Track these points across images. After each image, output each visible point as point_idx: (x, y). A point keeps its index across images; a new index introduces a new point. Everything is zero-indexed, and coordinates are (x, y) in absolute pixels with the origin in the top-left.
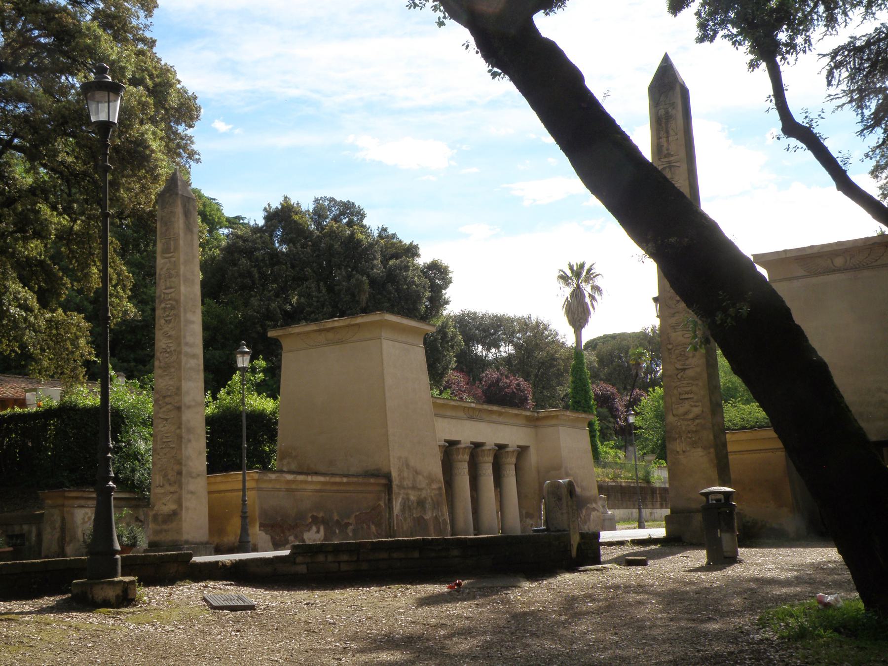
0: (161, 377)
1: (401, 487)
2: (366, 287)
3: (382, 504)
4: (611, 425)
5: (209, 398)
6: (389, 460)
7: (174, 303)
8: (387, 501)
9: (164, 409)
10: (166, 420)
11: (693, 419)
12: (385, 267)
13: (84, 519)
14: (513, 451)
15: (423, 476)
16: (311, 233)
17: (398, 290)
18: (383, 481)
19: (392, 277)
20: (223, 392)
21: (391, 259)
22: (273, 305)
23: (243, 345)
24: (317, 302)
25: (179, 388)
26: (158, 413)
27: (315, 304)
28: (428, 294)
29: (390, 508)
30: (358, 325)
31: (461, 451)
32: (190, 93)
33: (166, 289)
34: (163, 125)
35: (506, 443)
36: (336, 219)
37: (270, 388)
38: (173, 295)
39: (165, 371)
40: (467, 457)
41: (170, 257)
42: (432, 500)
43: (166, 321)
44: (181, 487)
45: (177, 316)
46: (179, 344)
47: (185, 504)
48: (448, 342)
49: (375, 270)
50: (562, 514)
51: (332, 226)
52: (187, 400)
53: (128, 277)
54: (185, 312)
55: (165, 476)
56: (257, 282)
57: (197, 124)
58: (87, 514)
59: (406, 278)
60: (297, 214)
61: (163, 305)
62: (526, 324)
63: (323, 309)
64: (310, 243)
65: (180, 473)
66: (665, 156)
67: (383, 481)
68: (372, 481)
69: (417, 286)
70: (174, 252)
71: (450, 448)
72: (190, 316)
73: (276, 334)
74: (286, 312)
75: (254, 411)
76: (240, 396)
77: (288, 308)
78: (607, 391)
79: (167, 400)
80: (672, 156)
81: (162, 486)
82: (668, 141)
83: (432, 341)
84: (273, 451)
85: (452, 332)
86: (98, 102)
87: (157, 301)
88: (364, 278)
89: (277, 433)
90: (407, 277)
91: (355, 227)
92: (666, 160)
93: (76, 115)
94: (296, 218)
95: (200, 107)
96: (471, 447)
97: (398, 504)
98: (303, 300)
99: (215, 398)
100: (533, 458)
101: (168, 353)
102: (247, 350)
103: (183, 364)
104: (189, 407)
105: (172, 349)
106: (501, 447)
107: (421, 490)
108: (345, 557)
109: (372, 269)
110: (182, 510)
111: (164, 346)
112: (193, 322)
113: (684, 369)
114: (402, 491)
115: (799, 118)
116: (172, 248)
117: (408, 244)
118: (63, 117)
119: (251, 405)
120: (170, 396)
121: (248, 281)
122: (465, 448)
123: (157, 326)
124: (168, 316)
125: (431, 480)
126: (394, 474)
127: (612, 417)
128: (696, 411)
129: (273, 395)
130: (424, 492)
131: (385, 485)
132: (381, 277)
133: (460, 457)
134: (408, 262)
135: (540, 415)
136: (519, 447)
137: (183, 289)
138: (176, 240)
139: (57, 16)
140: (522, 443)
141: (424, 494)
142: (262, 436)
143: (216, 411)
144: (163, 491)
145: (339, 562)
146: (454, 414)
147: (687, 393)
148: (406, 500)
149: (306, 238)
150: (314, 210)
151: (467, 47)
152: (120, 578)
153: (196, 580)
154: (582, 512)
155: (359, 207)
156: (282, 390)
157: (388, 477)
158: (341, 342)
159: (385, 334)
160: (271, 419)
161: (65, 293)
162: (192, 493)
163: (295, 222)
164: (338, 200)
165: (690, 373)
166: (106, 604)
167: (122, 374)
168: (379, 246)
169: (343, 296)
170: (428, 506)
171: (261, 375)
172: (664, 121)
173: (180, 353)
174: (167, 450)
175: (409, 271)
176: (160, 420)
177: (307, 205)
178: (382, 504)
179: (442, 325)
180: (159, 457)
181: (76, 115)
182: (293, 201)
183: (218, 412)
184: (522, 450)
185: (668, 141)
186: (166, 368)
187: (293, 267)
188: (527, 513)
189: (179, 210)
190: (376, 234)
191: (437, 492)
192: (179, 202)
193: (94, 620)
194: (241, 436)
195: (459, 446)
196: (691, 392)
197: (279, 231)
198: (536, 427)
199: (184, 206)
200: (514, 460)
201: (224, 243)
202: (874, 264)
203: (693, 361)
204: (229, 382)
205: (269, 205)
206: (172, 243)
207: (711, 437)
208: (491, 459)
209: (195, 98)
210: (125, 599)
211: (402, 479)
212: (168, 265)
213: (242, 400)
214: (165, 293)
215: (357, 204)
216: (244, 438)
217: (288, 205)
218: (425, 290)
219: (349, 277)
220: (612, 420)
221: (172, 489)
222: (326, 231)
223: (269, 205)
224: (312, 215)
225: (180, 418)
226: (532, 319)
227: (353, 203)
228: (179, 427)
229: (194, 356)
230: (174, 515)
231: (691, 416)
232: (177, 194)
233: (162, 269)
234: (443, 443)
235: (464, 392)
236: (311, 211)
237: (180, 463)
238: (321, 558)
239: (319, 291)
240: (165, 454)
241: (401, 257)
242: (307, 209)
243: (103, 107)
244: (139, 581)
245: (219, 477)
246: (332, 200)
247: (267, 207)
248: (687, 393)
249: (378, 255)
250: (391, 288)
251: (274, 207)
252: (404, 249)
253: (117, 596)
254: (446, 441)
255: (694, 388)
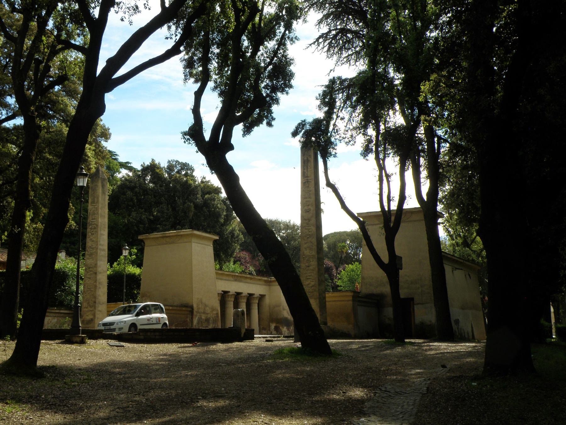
0: (88, 259)
1: (198, 312)
2: (193, 209)
3: (188, 320)
4: (329, 284)
5: (108, 266)
6: (193, 299)
7: (95, 226)
8: (191, 319)
9: (89, 273)
10: (90, 278)
11: (311, 287)
12: (203, 199)
13: (48, 322)
14: (257, 297)
15: (209, 308)
16: (165, 179)
17: (209, 211)
18: (189, 309)
19: (206, 204)
20: (115, 263)
21: (206, 194)
22: (144, 216)
23: (126, 245)
24: (167, 215)
25: (96, 264)
26: (86, 275)
27: (166, 217)
28: (225, 213)
29: (192, 322)
30: (181, 235)
31: (230, 296)
32: (107, 127)
33: (92, 219)
34: (94, 145)
35: (253, 293)
36: (179, 172)
37: (139, 263)
38: (95, 222)
39: (90, 256)
40: (233, 299)
41: (95, 205)
42: (213, 319)
43: (92, 234)
44: (95, 308)
45: (97, 232)
46: (97, 245)
47: (97, 316)
48: (235, 238)
49: (198, 200)
50: (239, 321)
51: (176, 176)
52: (99, 269)
53: (72, 209)
54: (101, 230)
55: (88, 303)
56: (136, 204)
57: (109, 141)
58: (49, 320)
59: (213, 205)
60: (158, 169)
61: (90, 227)
62: (288, 226)
63: (170, 219)
64: (164, 185)
65: (95, 302)
66: (306, 177)
67: (189, 309)
68: (184, 309)
69: (219, 209)
70: (97, 203)
71: (224, 295)
72: (102, 232)
73: (142, 238)
74: (150, 219)
75: (130, 274)
76: (124, 266)
77: (152, 217)
78: (329, 265)
79: (91, 269)
80: (309, 177)
81: (87, 308)
82: (307, 171)
83: (226, 238)
84: (138, 293)
85: (238, 233)
86: (80, 178)
87: (88, 225)
88: (192, 204)
89: (140, 284)
90: (214, 204)
91: (188, 177)
92: (306, 178)
93: (55, 141)
94: (158, 171)
95: (111, 134)
96: (235, 295)
97: (196, 320)
98: (159, 214)
99: (111, 267)
100: (267, 301)
101: (92, 248)
102: (127, 248)
103: (98, 253)
104: (100, 273)
105: (94, 247)
106: (251, 295)
107: (208, 314)
108: (157, 334)
109: (196, 200)
110: (95, 318)
111: (90, 245)
112: (104, 235)
113: (309, 266)
114: (198, 314)
115: (331, 181)
116: (96, 201)
117: (216, 186)
118: (50, 142)
119: (129, 271)
120: (92, 268)
121: (131, 203)
122: (232, 295)
123: (87, 236)
124: (92, 232)
125: (213, 309)
126: (195, 306)
127: (330, 279)
128: (313, 283)
129: (140, 265)
130: (209, 315)
131: (190, 311)
132: (201, 204)
133: (230, 299)
134: (215, 196)
135: (272, 280)
136: (260, 295)
137: (100, 220)
138: (98, 198)
139: (49, 95)
140: (262, 293)
141: (209, 316)
142: (134, 286)
143: (112, 273)
144: (87, 310)
145: (155, 336)
146: (227, 278)
147: (309, 276)
148: (200, 318)
149: (162, 182)
150: (167, 166)
151: (203, 165)
152: (80, 335)
153: (105, 339)
154: (290, 328)
155: (191, 166)
156: (144, 265)
157: (192, 307)
158: (173, 243)
159: (194, 240)
160: (138, 278)
161: (42, 215)
162: (100, 311)
163: (157, 173)
164: (180, 161)
165: (311, 268)
166: (76, 343)
167: (64, 251)
168: (200, 187)
169: (180, 213)
170: (210, 322)
171: (134, 256)
172: (306, 162)
173: (97, 248)
174: (90, 292)
175: (215, 201)
176: (87, 278)
177: (164, 164)
178: (188, 320)
179: (232, 229)
180: (86, 295)
181: (55, 141)
182: (157, 162)
183: (113, 274)
184: (262, 297)
185: (307, 171)
186: (91, 255)
187: (155, 196)
188: (263, 328)
189: (100, 184)
190: (200, 181)
191: (216, 315)
192: (100, 181)
193: (74, 347)
194: (123, 286)
195: (229, 294)
196: (311, 276)
197: (148, 177)
198: (269, 285)
199: (102, 183)
200: (257, 301)
201: (119, 183)
202: (407, 220)
203: (312, 263)
204: (119, 259)
205: (144, 163)
206: (96, 199)
207: (318, 294)
208: (245, 300)
209: (109, 129)
210: (82, 342)
211: (198, 308)
212: (94, 209)
213: (125, 268)
214: (91, 222)
215: (190, 164)
216: (125, 287)
217: (154, 164)
218: (223, 211)
219: (184, 203)
220: (330, 281)
221: (91, 309)
222: (173, 178)
223: (144, 163)
224: (166, 169)
225: (96, 278)
226: (291, 223)
227: (188, 164)
228: (96, 282)
229: (104, 250)
230: (92, 321)
231: (310, 285)
232: (99, 177)
233: (91, 210)
234: (220, 292)
235: (248, 263)
236: (166, 167)
237: (95, 297)
238: (149, 334)
239: (168, 210)
240: (89, 294)
241: (212, 194)
242: (163, 166)
243: (81, 180)
244: (87, 336)
245: (112, 304)
246: (177, 161)
247: (143, 164)
248: (309, 276)
249: (200, 193)
250: (205, 210)
251: (146, 164)
252: (214, 189)
253: (80, 341)
254: (222, 291)
255: (312, 274)
